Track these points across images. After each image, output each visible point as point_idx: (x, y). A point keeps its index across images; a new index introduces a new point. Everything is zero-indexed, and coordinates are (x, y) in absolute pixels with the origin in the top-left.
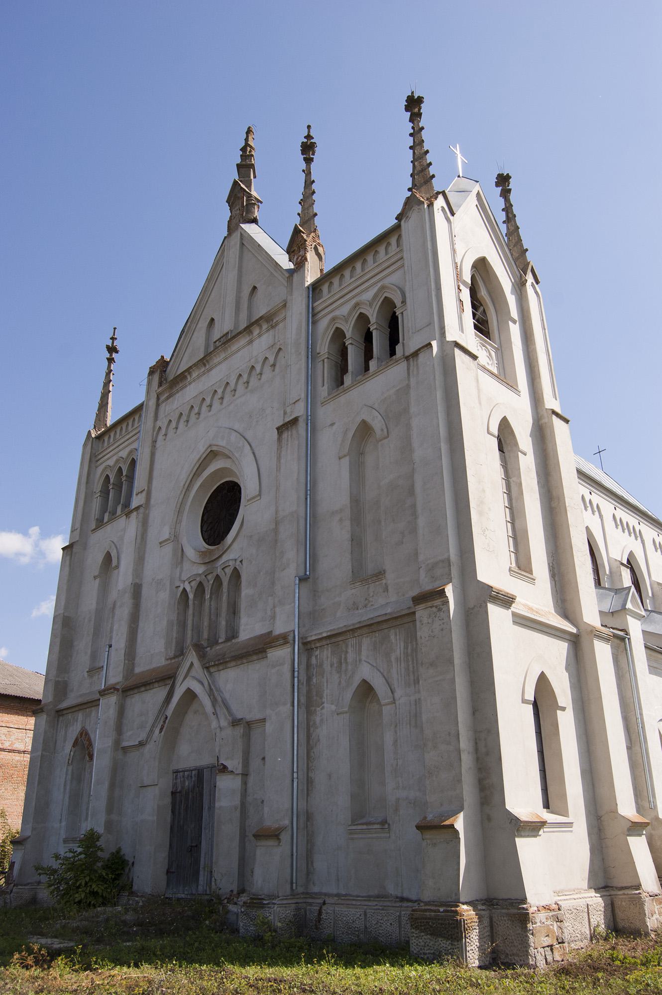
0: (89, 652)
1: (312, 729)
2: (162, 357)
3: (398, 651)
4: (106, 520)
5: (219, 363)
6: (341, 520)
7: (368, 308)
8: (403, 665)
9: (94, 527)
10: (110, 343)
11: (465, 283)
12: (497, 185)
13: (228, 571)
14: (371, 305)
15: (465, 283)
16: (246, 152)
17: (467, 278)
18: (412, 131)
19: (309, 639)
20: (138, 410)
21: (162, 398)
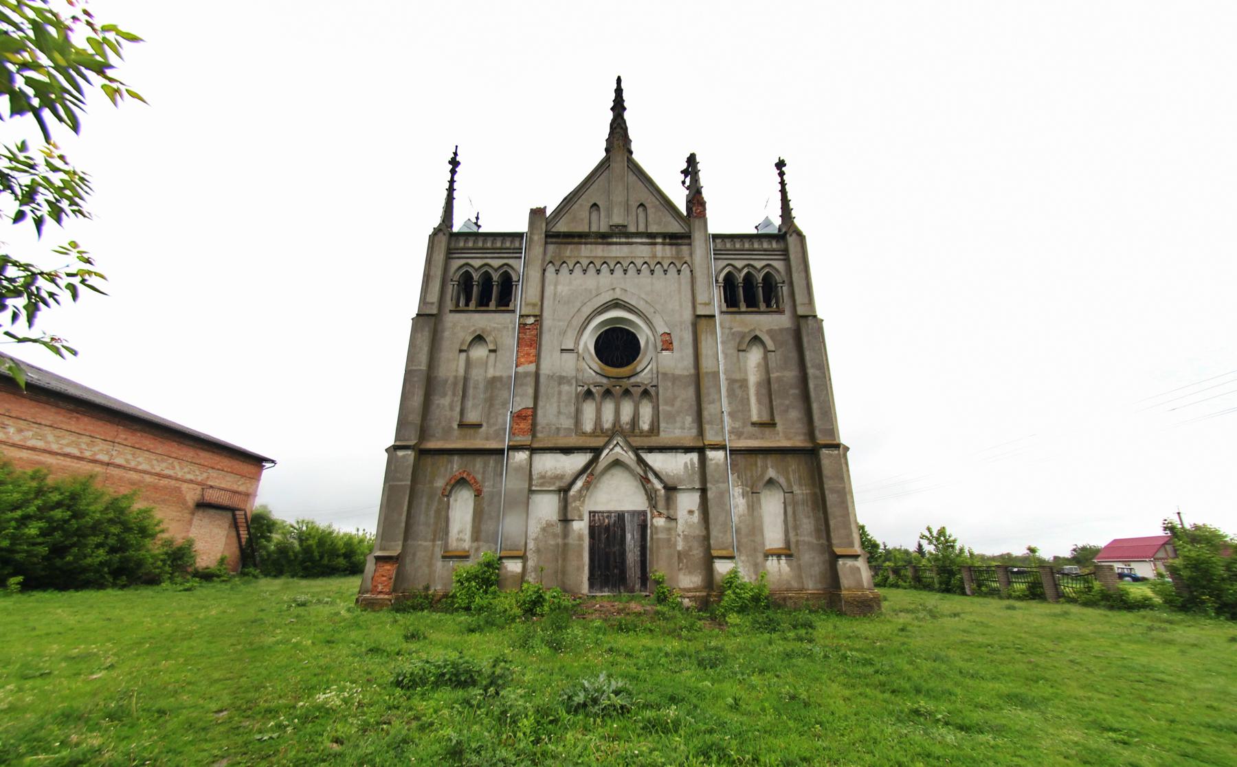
5: (616, 244)
16: (619, 91)
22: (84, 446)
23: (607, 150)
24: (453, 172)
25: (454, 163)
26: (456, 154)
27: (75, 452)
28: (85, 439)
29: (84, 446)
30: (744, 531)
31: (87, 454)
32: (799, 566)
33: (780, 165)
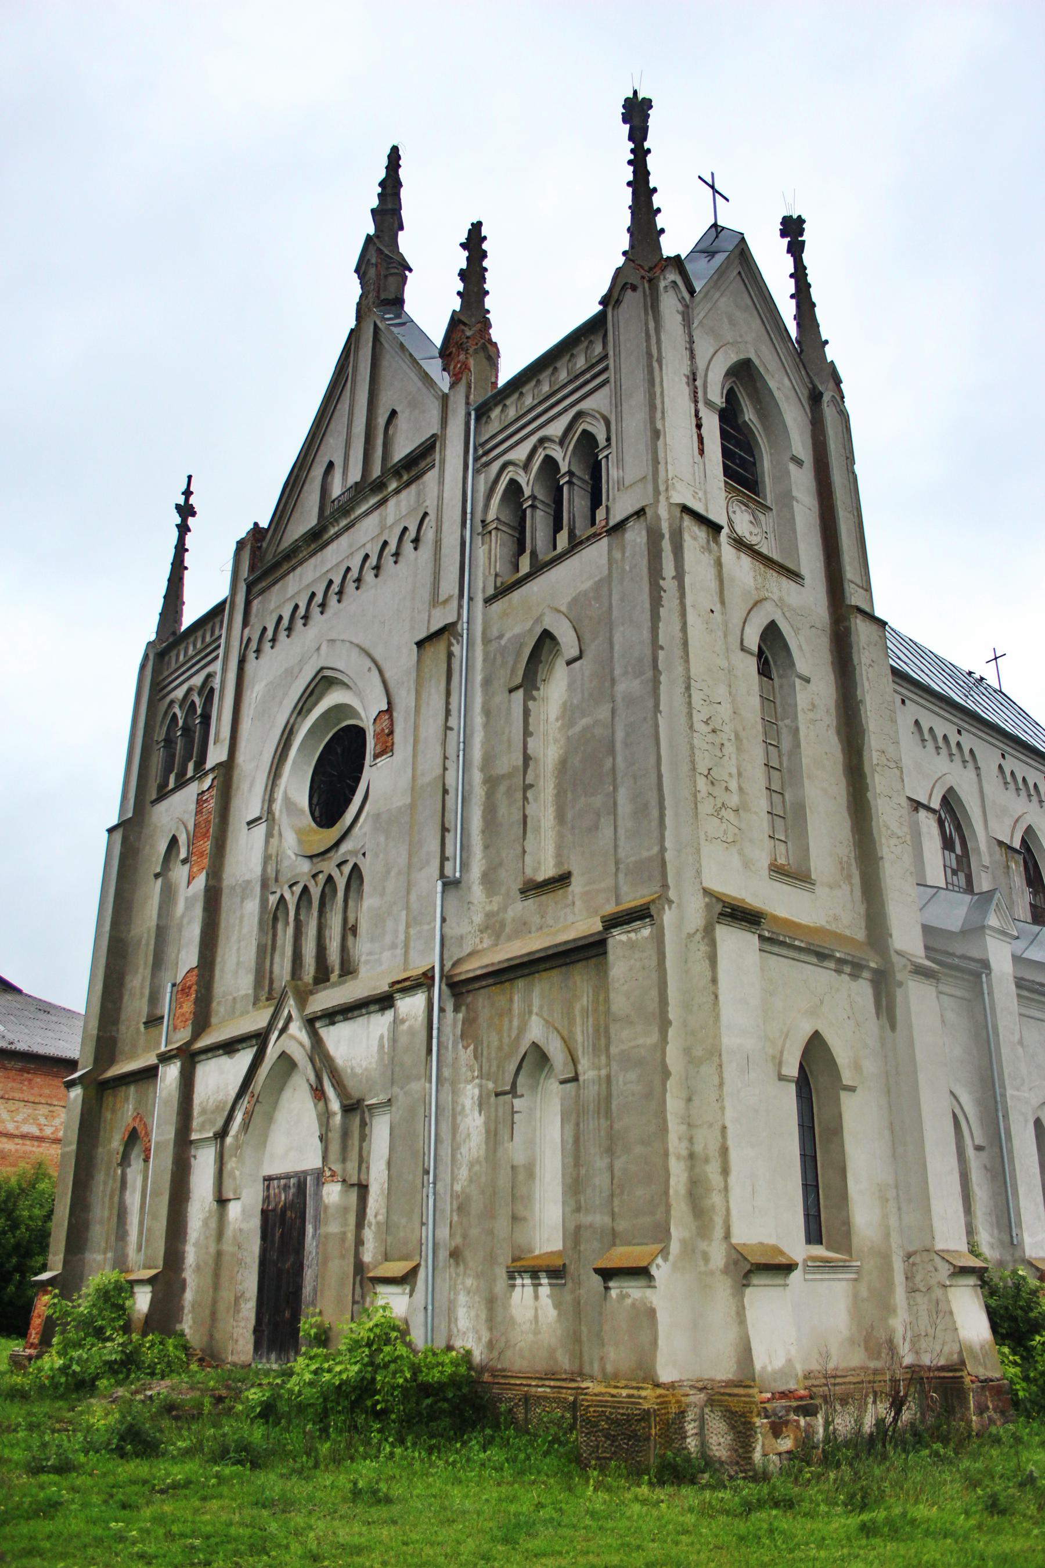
0: (147, 992)
1: (459, 1118)
2: (256, 524)
3: (585, 999)
4: (190, 773)
5: (337, 536)
6: (509, 788)
7: (558, 448)
8: (591, 1020)
9: (154, 797)
10: (181, 500)
11: (709, 404)
12: (783, 234)
13: (347, 869)
14: (561, 443)
15: (709, 404)
16: (391, 186)
17: (717, 397)
18: (632, 157)
19: (971, 978)
20: (218, 610)
21: (256, 589)
22: (42, 1121)
23: (605, 301)
24: (183, 529)
25: (186, 511)
26: (188, 493)
27: (34, 1130)
28: (43, 1110)
29: (42, 1121)
30: (476, 1206)
31: (48, 1131)
32: (577, 1303)
33: (636, 113)
